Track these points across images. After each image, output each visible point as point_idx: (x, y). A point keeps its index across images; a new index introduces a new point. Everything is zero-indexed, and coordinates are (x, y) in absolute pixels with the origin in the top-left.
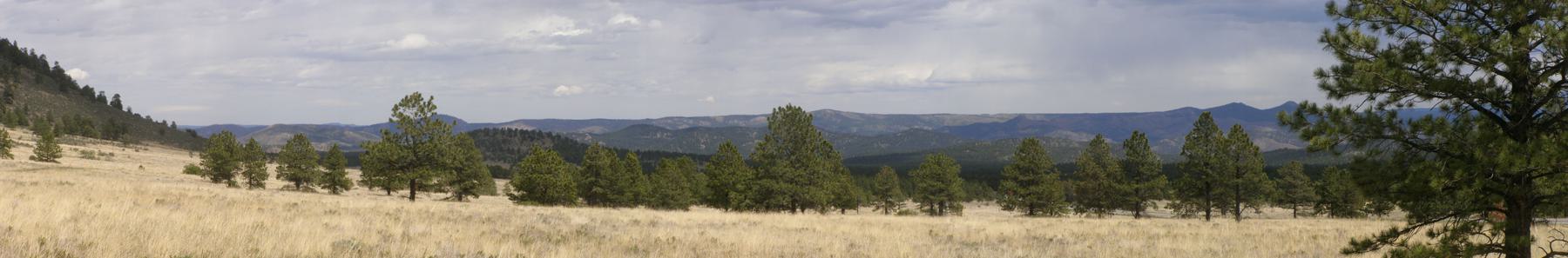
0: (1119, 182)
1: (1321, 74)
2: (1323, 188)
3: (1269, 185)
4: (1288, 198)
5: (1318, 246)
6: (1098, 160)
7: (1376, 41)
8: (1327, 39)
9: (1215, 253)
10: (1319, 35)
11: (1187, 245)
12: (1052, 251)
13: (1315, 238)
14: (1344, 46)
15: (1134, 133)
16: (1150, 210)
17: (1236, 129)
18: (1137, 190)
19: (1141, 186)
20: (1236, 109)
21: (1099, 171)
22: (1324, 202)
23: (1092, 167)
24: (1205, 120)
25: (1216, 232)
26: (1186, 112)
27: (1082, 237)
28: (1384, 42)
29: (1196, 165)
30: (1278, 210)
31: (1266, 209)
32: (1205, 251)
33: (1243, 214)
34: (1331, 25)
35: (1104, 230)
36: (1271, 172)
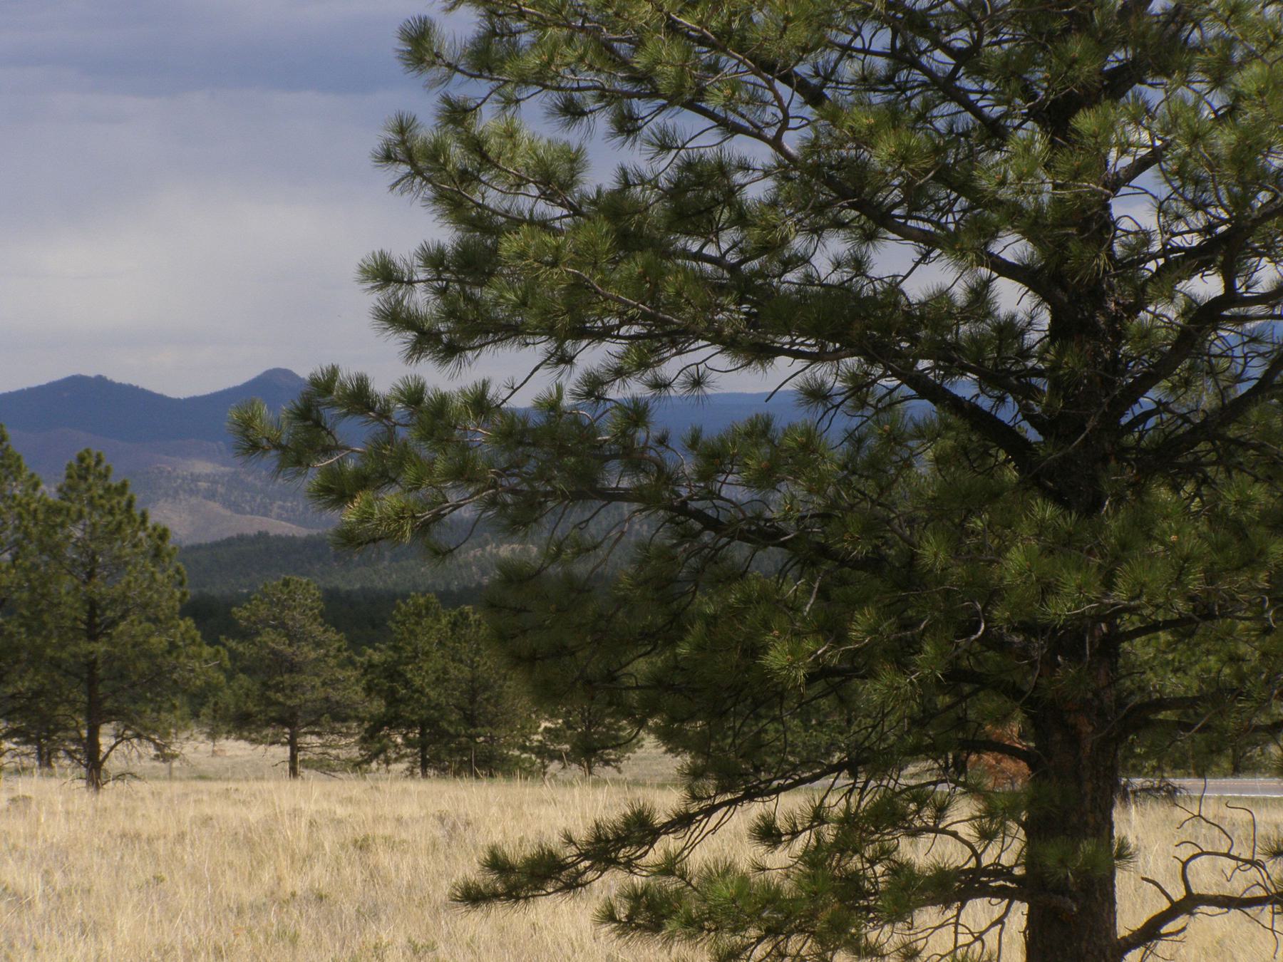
1: (384, 273)
2: (392, 672)
3: (202, 663)
4: (269, 708)
5: (374, 875)
7: (574, 160)
10: (378, 137)
13: (363, 845)
14: (466, 177)
17: (84, 470)
22: (393, 721)
30: (235, 748)
31: (194, 747)
33: (113, 764)
36: (211, 617)
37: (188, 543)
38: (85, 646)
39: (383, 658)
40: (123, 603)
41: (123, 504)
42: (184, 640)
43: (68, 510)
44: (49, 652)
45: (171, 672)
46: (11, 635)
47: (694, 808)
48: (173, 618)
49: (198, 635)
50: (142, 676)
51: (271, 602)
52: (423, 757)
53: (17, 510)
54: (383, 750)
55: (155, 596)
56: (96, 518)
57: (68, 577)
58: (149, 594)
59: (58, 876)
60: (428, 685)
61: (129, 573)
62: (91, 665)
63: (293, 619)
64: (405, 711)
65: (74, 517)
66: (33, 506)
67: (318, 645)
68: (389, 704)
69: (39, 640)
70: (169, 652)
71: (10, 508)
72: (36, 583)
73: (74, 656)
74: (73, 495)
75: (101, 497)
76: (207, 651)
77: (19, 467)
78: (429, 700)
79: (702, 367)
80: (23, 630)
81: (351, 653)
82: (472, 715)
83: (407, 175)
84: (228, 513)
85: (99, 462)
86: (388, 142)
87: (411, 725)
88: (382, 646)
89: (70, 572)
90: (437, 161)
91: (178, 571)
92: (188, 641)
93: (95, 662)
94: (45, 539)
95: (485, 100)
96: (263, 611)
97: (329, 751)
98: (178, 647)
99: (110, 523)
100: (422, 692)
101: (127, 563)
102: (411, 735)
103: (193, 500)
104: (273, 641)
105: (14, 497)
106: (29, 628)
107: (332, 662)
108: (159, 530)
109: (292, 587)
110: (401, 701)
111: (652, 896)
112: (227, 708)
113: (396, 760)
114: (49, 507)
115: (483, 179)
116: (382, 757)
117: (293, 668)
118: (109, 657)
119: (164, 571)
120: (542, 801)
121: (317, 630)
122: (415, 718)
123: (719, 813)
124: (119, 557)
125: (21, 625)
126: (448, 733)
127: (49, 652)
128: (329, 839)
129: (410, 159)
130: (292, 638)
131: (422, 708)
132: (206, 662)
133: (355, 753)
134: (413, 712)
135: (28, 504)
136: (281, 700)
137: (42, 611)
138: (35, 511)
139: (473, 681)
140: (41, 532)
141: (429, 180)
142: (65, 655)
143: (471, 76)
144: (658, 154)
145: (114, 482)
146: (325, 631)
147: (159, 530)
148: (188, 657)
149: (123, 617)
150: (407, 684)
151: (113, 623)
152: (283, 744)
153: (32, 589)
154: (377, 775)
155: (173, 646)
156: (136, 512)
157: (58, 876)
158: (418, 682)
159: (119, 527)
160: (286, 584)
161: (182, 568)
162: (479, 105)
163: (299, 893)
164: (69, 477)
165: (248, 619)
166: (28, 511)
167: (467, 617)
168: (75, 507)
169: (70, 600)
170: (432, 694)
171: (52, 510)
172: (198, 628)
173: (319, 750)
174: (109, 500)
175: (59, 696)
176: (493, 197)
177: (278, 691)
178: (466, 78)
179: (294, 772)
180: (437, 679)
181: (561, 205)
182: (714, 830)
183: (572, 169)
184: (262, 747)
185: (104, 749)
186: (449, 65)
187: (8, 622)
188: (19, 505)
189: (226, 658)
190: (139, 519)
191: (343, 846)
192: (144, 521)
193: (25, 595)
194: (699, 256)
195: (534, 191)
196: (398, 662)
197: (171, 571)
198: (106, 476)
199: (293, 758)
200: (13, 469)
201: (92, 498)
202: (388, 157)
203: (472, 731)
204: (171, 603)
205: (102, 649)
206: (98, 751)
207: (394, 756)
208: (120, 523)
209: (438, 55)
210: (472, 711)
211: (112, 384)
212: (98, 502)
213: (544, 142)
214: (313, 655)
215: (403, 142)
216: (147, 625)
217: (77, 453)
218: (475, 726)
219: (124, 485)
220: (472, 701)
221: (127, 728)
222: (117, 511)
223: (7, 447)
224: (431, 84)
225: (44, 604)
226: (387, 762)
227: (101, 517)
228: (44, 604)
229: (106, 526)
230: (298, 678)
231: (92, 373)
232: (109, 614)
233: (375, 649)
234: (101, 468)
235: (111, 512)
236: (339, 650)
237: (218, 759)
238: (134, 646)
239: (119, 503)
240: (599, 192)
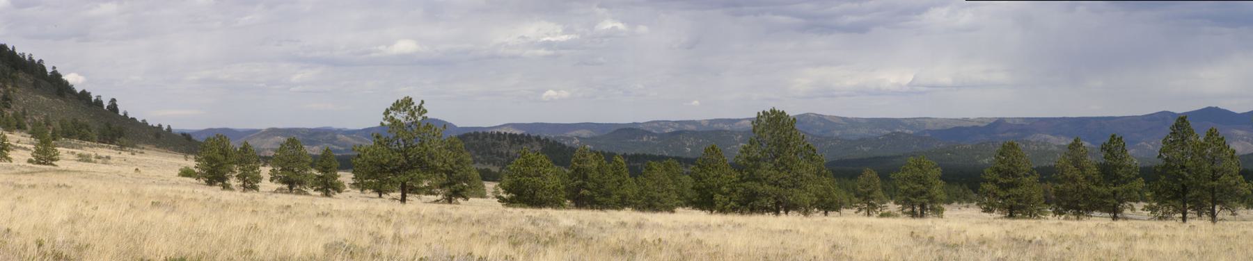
0: (1097, 185)
6: (1076, 163)
11: (1164, 247)
12: (1031, 253)
16: (1127, 212)
17: (1212, 133)
18: (1115, 193)
20: (1213, 114)
21: (1077, 173)
23: (1071, 170)
24: (1181, 124)
25: (1192, 233)
27: (1059, 239)
33: (1219, 216)
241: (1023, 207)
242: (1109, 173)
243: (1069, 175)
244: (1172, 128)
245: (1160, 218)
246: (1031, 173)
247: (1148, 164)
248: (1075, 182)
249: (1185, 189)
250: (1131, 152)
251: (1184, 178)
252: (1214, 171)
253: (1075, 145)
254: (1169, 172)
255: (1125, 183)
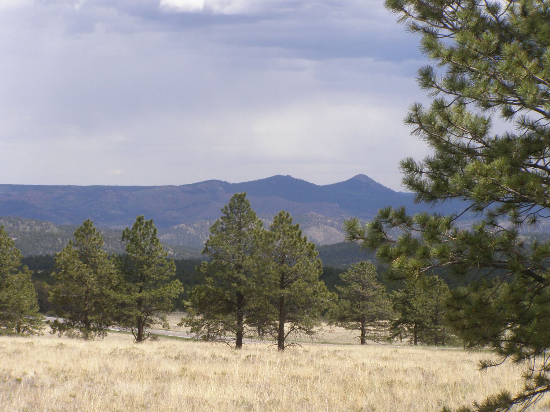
0: (115, 288)
1: (409, 166)
2: (405, 302)
3: (326, 297)
4: (355, 314)
5: (394, 398)
6: (86, 257)
7: (487, 123)
8: (416, 118)
9: (250, 407)
10: (406, 111)
11: (209, 392)
12: (20, 401)
13: (390, 384)
14: (442, 130)
15: (141, 213)
16: (156, 328)
17: (281, 220)
18: (140, 302)
19: (145, 294)
20: (283, 186)
21: (86, 271)
22: (404, 321)
23: (78, 267)
24: (238, 202)
25: (250, 370)
26: (211, 188)
27: (61, 376)
28: (501, 127)
29: (223, 268)
30: (339, 330)
31: (323, 329)
32: (236, 403)
33: (290, 338)
34: (426, 101)
35: (92, 364)
36: (331, 277)
37: (322, 244)
38: (279, 291)
39: (401, 295)
40: (295, 274)
41: (297, 234)
42: (320, 289)
43: (275, 236)
44: (265, 293)
45: (314, 302)
46: (249, 285)
47: (527, 393)
48: (316, 281)
49: (326, 288)
50: (302, 304)
51: (356, 272)
52: (415, 336)
53: (254, 234)
54: (399, 333)
55: (309, 272)
56: (285, 239)
57: (274, 263)
58: (306, 270)
59: (266, 395)
60: (419, 307)
61: (298, 262)
62: (282, 299)
63: (364, 279)
64: (409, 318)
65: (277, 238)
66: (260, 233)
67: (375, 290)
68: (403, 315)
69: (260, 288)
70: (314, 294)
71: (250, 234)
72: (261, 265)
73: (275, 295)
74: (277, 229)
75: (288, 231)
76: (329, 294)
77: (255, 217)
78: (419, 314)
79: (536, 214)
80: (254, 283)
81: (388, 293)
82: (436, 320)
83: (418, 128)
84: (339, 232)
85: (287, 216)
86: (410, 115)
87: (411, 323)
88: (401, 291)
89: (274, 261)
90: (431, 124)
91: (318, 262)
92: (322, 290)
93: (283, 297)
94: (265, 247)
95: (452, 103)
96: (352, 275)
97: (377, 332)
98: (318, 292)
99: (291, 241)
100: (416, 309)
101: (297, 258)
102: (411, 327)
103: (325, 227)
104: (356, 287)
105: (253, 230)
106: (257, 282)
107: (380, 297)
108: (311, 244)
109: (364, 266)
110: (407, 313)
111: (504, 206)
112: (336, 314)
113: (405, 337)
114: (267, 234)
115: (449, 130)
116: (399, 335)
117: (364, 299)
118: (289, 296)
119: (312, 262)
120: (463, 361)
121: (374, 283)
122: (413, 320)
123: (536, 396)
124: (295, 255)
125: (253, 282)
126: (427, 327)
127: (265, 293)
128: (377, 379)
129: (419, 122)
130: (364, 287)
131: (416, 316)
132: (329, 299)
133: (388, 334)
134: (412, 318)
135: (258, 232)
136: (359, 311)
137: (262, 276)
138: (261, 235)
139: (437, 306)
140: (263, 244)
141: (427, 131)
142: (271, 295)
143: (447, 93)
144: (521, 127)
145: (294, 225)
146: (377, 285)
147: (311, 244)
148: (321, 296)
149: (295, 280)
150: (410, 306)
151: (291, 282)
152: (359, 329)
153: (258, 267)
154: (396, 344)
155: (315, 292)
156: (302, 237)
157: (266, 395)
158: (415, 305)
159: (295, 243)
160: (362, 264)
161: (320, 260)
162: (449, 105)
163: (364, 407)
164: (275, 222)
165: (345, 279)
166: (258, 236)
167: (436, 280)
168: (277, 234)
169: (274, 272)
170: (420, 310)
171: (268, 235)
172: (326, 285)
173: (373, 332)
174: (291, 232)
175: (268, 311)
176: (453, 138)
177: (357, 308)
178: (445, 93)
179: (363, 342)
180: (423, 305)
181: (480, 142)
182: (535, 402)
183: (486, 127)
184: (350, 330)
185: (286, 333)
186: (438, 88)
187: (248, 280)
188: (255, 232)
189: (337, 298)
190: (303, 241)
191: (382, 384)
192: (305, 241)
193: (256, 269)
194: (535, 166)
195: (469, 136)
196: (407, 298)
197: (316, 262)
198: (290, 222)
199: (363, 335)
200: (252, 218)
201: (285, 231)
202: (410, 121)
203: (436, 326)
204: (315, 275)
205: (287, 293)
206: (283, 334)
207: (404, 336)
208: (296, 242)
209: (434, 82)
210: (436, 319)
211: (293, 178)
212: (287, 233)
213: (474, 115)
214: (372, 294)
215: (417, 115)
216: (306, 283)
217: (279, 212)
218: (437, 325)
219: (298, 226)
220: (436, 314)
221: (295, 324)
222: (295, 237)
223: (250, 209)
224: (431, 95)
225: (263, 274)
226: (401, 338)
227: (288, 239)
228: (263, 274)
229: (290, 242)
230: (365, 303)
231: (285, 174)
232: (290, 278)
233: (398, 291)
234: (289, 219)
235: (292, 237)
236: (383, 292)
237: (332, 334)
238: (299, 292)
239: (295, 233)
240: (496, 138)
241: (9, 318)
242: (132, 270)
243: (75, 274)
244: (225, 210)
245: (206, 338)
246: (20, 268)
247: (188, 256)
248: (84, 283)
249: (241, 299)
250: (163, 237)
251: (240, 283)
252: (283, 274)
253: (85, 230)
254: (220, 274)
255: (155, 286)
